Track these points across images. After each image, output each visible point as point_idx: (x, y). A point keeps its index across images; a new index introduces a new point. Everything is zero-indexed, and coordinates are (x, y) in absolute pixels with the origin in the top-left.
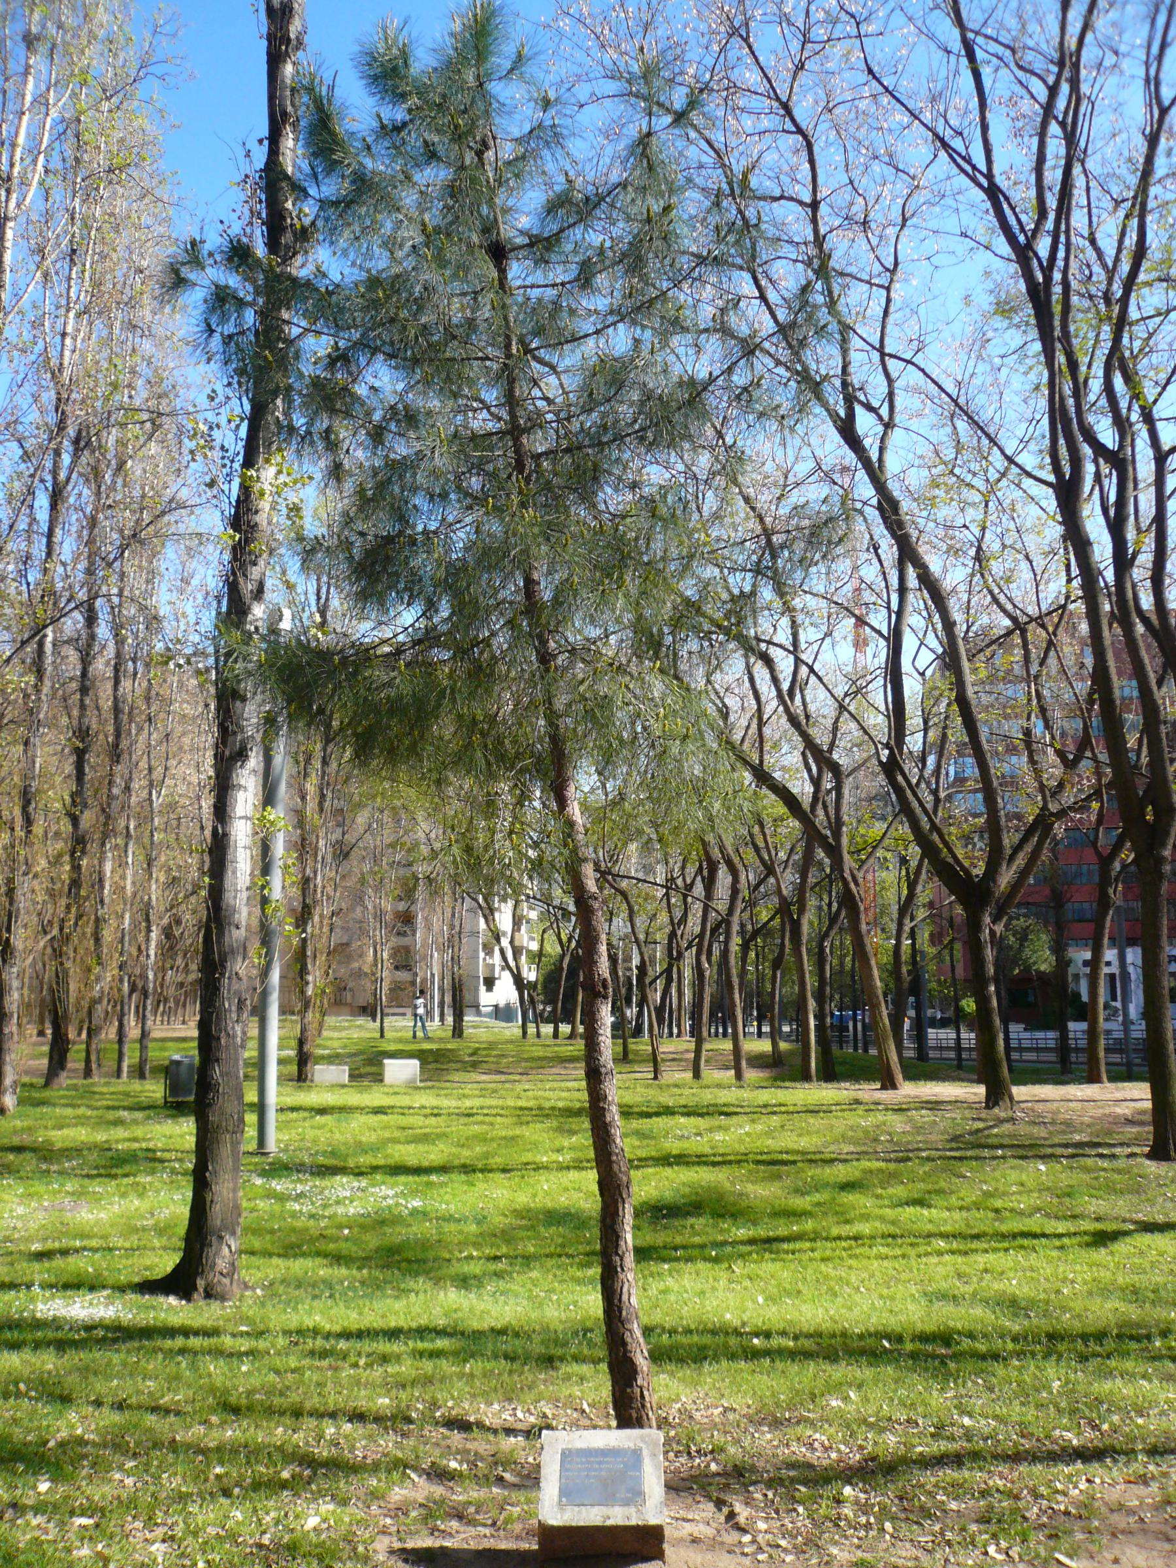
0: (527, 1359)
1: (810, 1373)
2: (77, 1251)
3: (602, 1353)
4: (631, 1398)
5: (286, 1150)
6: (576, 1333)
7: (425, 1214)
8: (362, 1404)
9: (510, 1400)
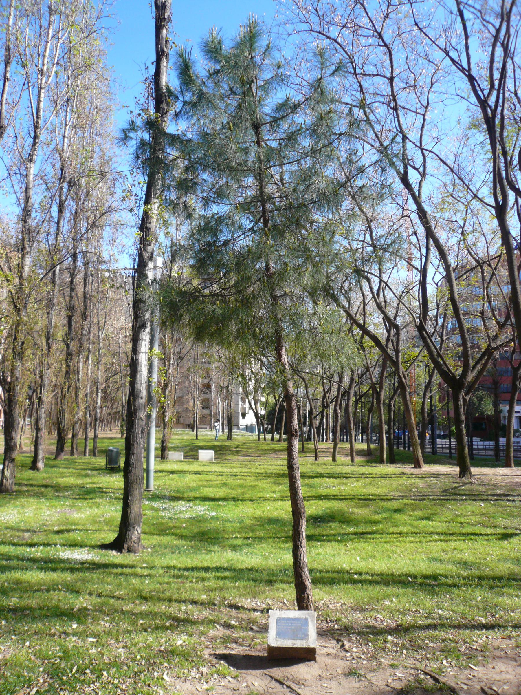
0: (261, 581)
1: (376, 591)
2: (73, 530)
3: (292, 579)
4: (304, 599)
5: (157, 489)
6: (281, 571)
7: (217, 519)
8: (196, 598)
9: (255, 598)
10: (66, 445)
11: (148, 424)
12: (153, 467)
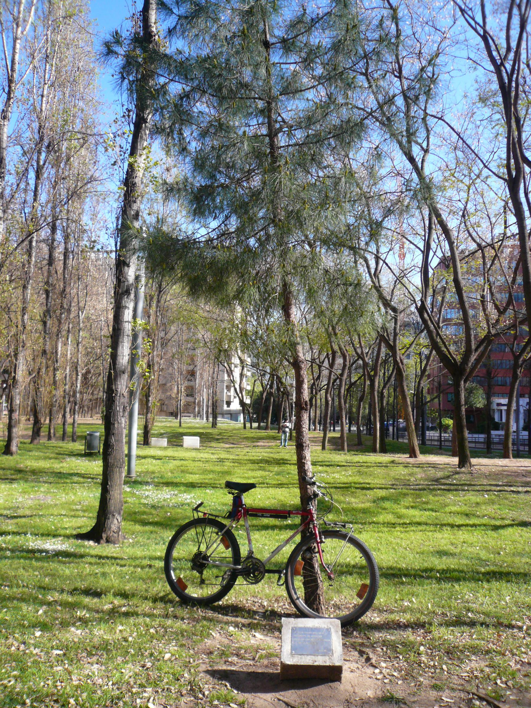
10: (42, 429)
11: (131, 403)
12: (135, 451)
